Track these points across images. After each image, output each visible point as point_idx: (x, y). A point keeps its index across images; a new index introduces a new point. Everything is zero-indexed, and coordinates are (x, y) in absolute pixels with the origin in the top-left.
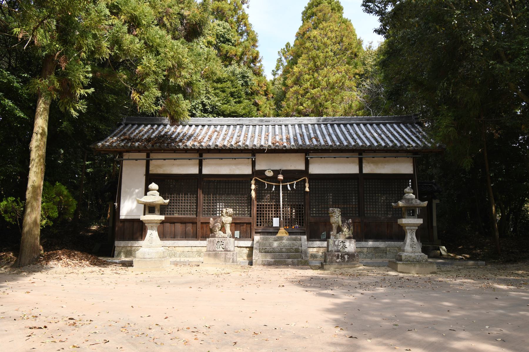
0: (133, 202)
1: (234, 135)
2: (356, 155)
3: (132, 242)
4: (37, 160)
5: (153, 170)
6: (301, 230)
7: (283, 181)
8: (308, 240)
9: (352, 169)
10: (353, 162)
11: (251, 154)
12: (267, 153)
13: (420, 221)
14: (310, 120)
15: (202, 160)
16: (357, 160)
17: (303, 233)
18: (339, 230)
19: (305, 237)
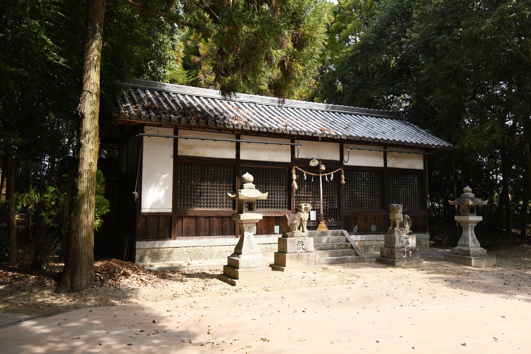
0: (160, 191)
2: (381, 148)
3: (158, 242)
4: (93, 133)
5: (183, 151)
6: (337, 223)
7: (326, 171)
9: (378, 162)
10: (379, 156)
11: (290, 140)
12: (321, 141)
13: (480, 218)
14: (319, 106)
15: (294, 145)
16: (382, 154)
18: (402, 226)
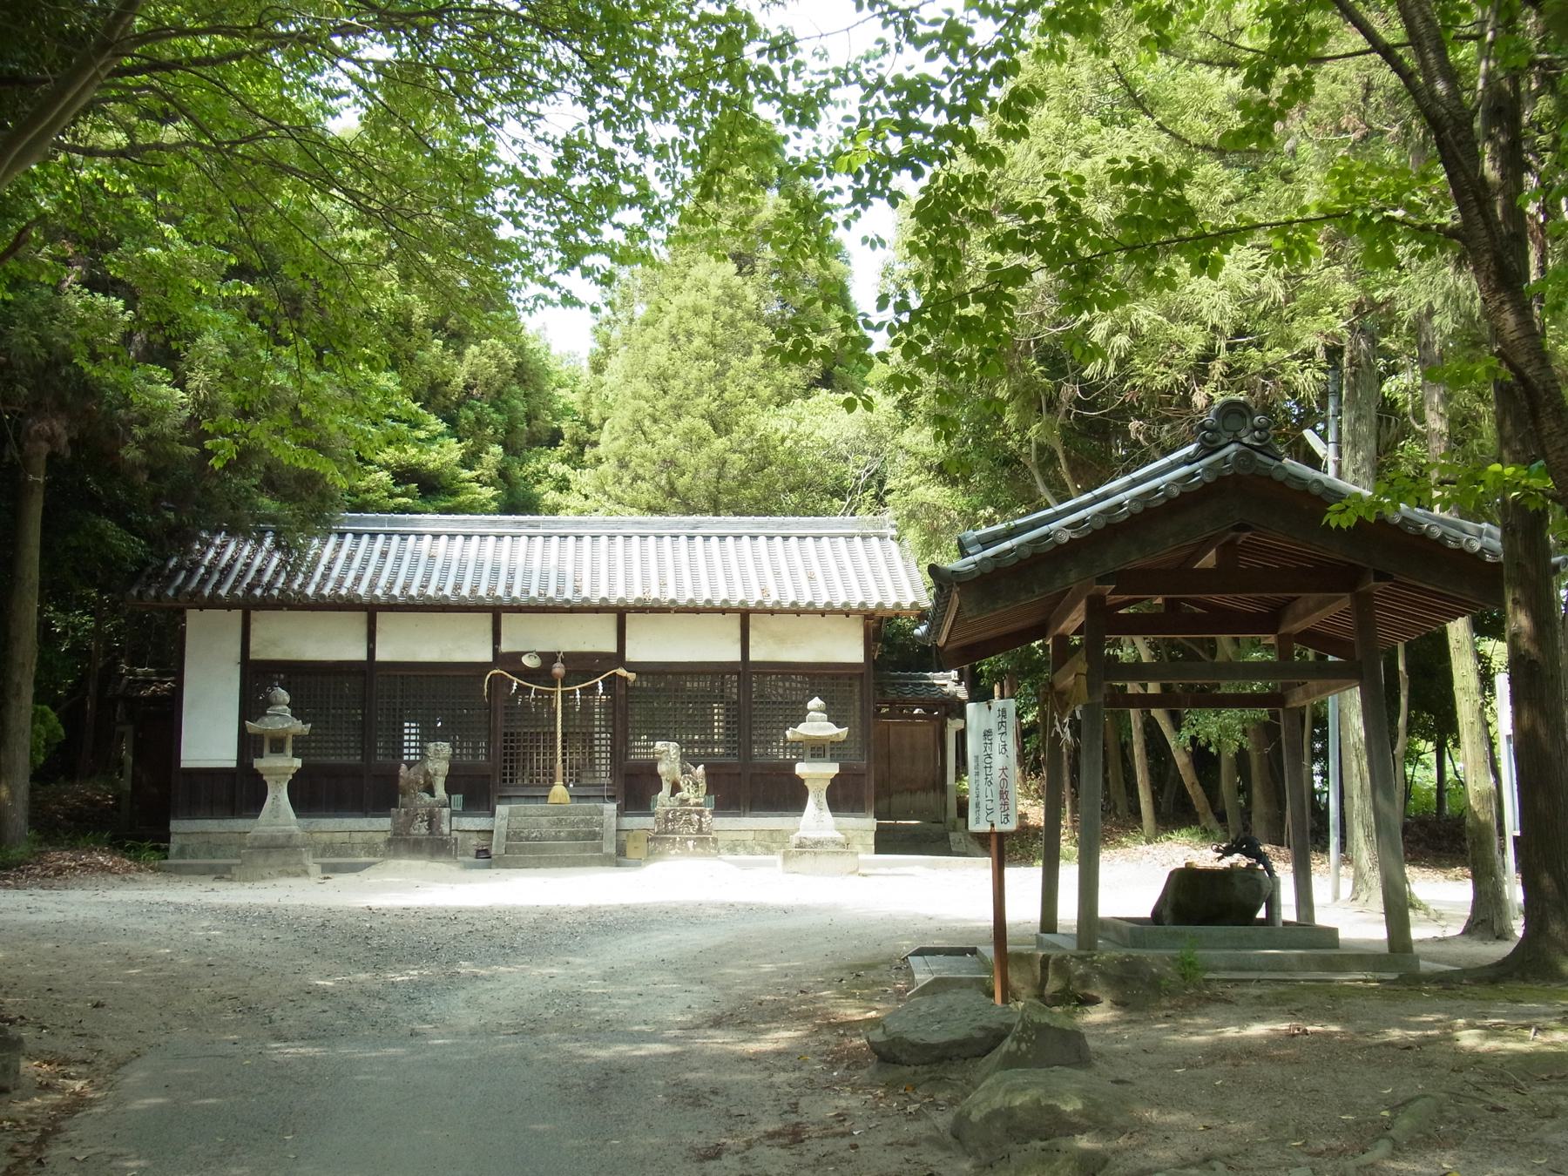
1: (428, 581)
5: (259, 652)
8: (622, 812)
17: (612, 798)
19: (614, 806)
